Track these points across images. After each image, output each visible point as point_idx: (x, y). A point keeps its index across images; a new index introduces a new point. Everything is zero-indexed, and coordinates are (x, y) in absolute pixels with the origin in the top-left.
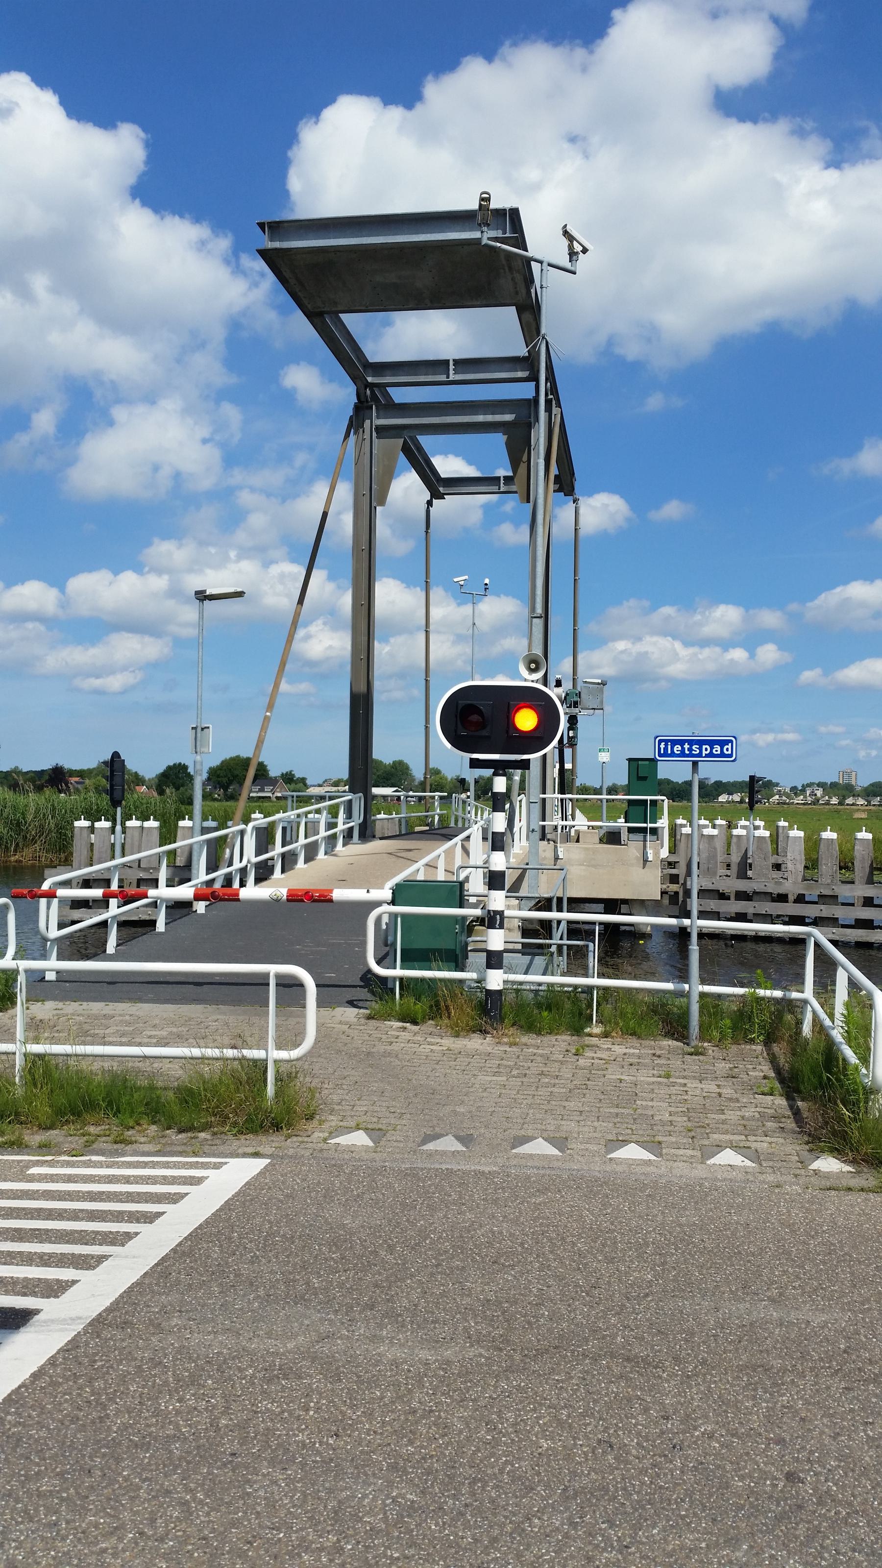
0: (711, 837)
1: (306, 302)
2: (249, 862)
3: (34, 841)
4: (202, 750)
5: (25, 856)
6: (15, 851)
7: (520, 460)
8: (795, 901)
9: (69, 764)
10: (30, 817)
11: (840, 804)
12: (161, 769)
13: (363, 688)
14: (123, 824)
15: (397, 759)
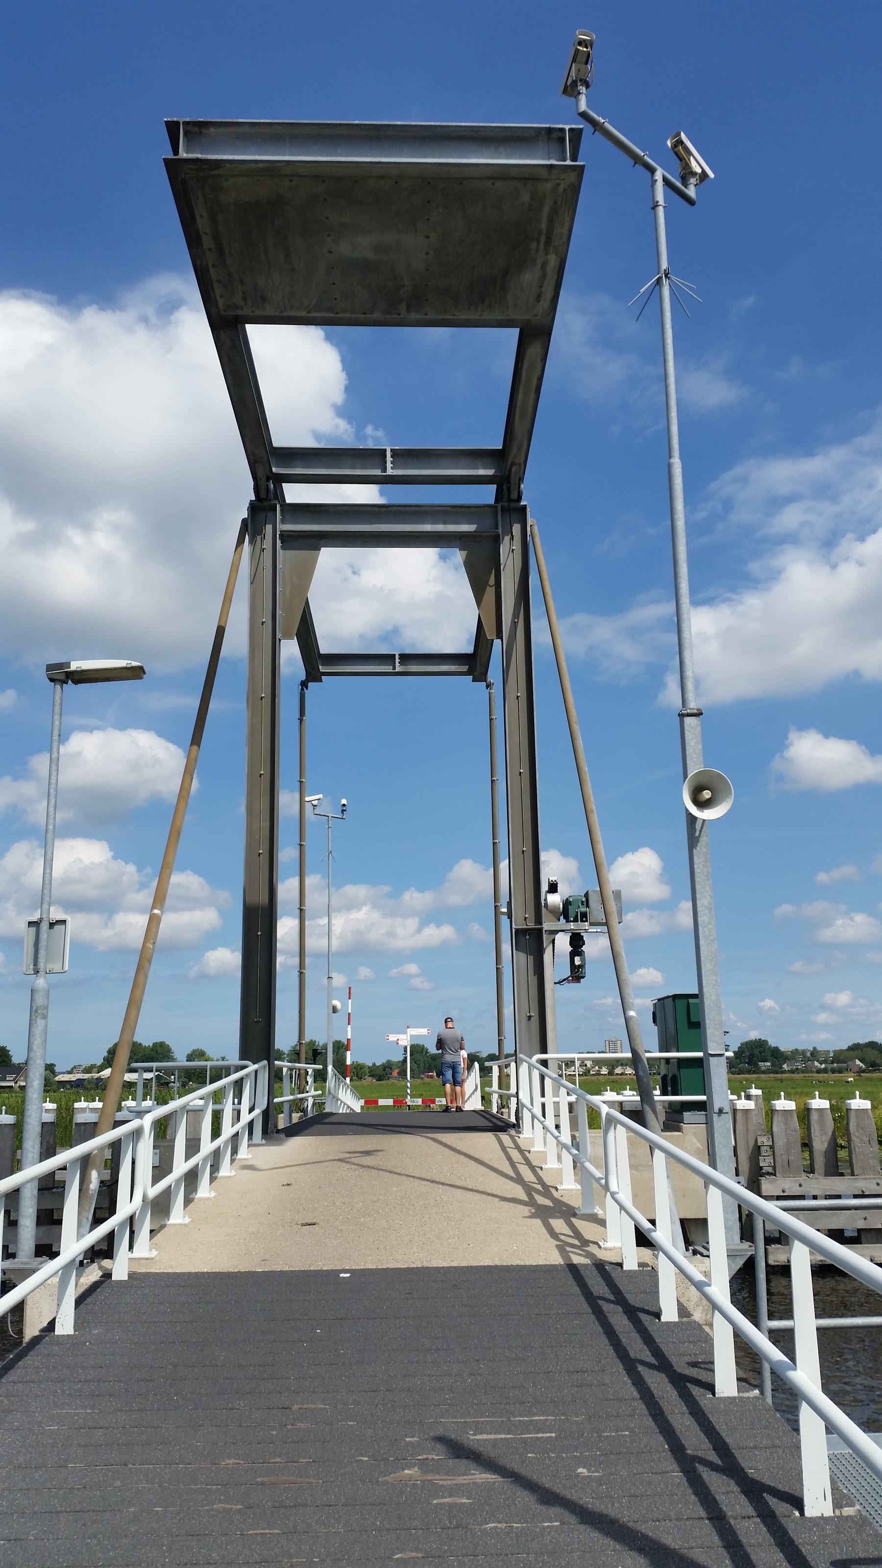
1: (218, 290)
4: (50, 966)
7: (486, 584)
11: (611, 1073)
13: (263, 898)
15: (158, 1041)
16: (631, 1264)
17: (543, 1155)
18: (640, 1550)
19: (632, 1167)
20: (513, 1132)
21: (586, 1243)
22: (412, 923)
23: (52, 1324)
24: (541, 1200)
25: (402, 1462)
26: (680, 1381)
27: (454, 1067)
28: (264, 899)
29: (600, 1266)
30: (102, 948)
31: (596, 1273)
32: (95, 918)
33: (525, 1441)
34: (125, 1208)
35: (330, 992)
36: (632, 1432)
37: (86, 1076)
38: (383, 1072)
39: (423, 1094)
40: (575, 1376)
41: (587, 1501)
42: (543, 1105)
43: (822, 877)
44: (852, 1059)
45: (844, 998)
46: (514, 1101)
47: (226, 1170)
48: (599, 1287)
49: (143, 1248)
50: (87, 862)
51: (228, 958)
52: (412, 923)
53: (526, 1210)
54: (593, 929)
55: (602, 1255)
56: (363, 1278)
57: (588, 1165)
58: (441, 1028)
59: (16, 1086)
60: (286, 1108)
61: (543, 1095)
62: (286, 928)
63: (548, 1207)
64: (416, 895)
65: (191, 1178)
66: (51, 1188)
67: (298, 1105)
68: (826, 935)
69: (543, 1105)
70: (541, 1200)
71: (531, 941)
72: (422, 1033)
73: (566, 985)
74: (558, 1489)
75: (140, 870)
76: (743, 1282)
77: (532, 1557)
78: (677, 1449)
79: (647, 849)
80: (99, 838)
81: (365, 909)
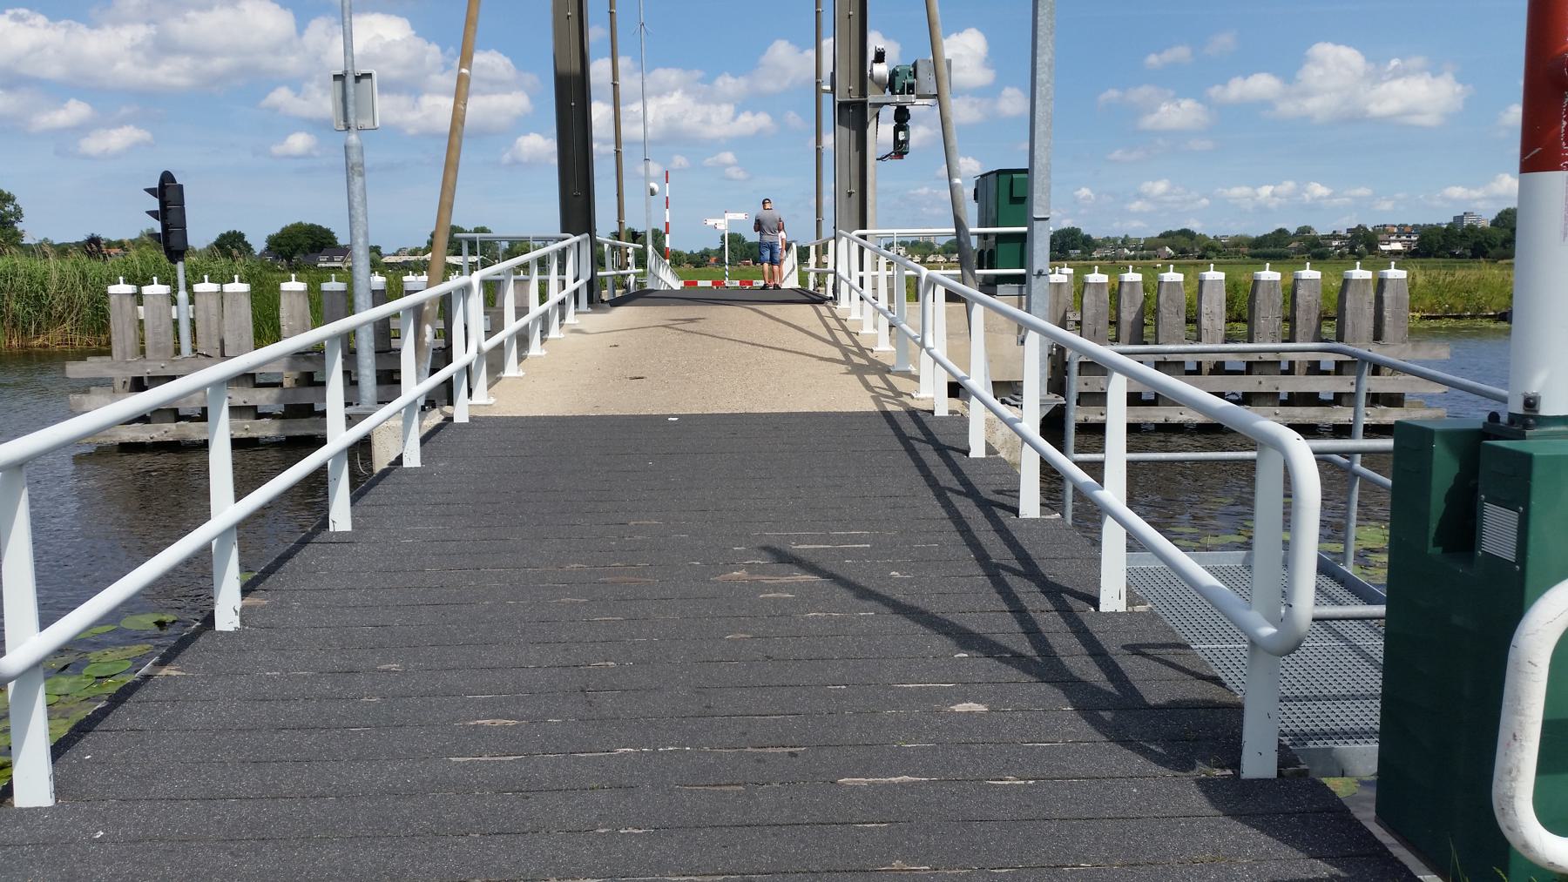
0: (1059, 285)
2: (479, 351)
3: (61, 319)
4: (361, 123)
5: (53, 338)
6: (37, 332)
8: (1212, 372)
9: (109, 233)
10: (52, 289)
12: (213, 239)
14: (189, 287)
16: (942, 411)
17: (860, 323)
18: (947, 634)
19: (948, 335)
20: (830, 304)
21: (900, 394)
22: (727, 110)
23: (399, 460)
24: (856, 360)
25: (731, 565)
26: (986, 506)
27: (772, 247)
28: (575, 67)
29: (913, 413)
30: (411, 131)
31: (909, 418)
32: (403, 101)
33: (842, 550)
34: (460, 358)
35: (647, 178)
36: (941, 544)
37: (413, 258)
38: (700, 260)
39: (742, 269)
40: (888, 500)
41: (899, 596)
42: (861, 279)
43: (1153, 59)
44: (1163, 246)
45: (1161, 187)
46: (831, 278)
47: (554, 332)
48: (911, 429)
49: (481, 396)
50: (388, 39)
51: (542, 145)
52: (727, 110)
53: (843, 368)
54: (919, 102)
55: (914, 404)
56: (689, 422)
57: (904, 326)
58: (758, 210)
59: (344, 267)
60: (609, 283)
61: (861, 269)
62: (600, 112)
63: (862, 364)
64: (730, 80)
65: (523, 339)
66: (385, 332)
67: (620, 282)
68: (1149, 122)
69: (861, 279)
70: (856, 360)
71: (854, 115)
72: (735, 220)
73: (889, 161)
74: (872, 586)
75: (443, 51)
76: (1053, 426)
77: (849, 638)
78: (982, 558)
79: (973, 30)
80: (400, 15)
81: (677, 95)
